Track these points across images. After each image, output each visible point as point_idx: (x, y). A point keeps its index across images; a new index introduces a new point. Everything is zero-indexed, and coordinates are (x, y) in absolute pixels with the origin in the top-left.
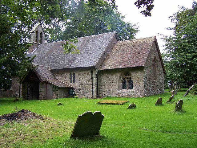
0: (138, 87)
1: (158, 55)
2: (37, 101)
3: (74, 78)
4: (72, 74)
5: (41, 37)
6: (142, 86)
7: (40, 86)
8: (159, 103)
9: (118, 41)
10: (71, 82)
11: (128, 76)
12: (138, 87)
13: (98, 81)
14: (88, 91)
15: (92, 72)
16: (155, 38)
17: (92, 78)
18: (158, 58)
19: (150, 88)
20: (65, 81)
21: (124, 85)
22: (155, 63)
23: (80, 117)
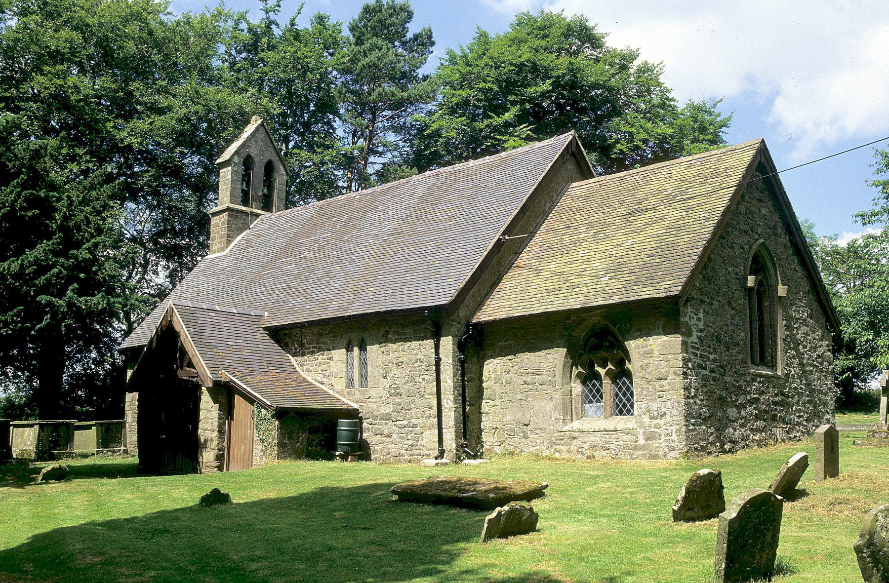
0: (654, 406)
1: (784, 239)
10: (350, 383)
21: (624, 395)
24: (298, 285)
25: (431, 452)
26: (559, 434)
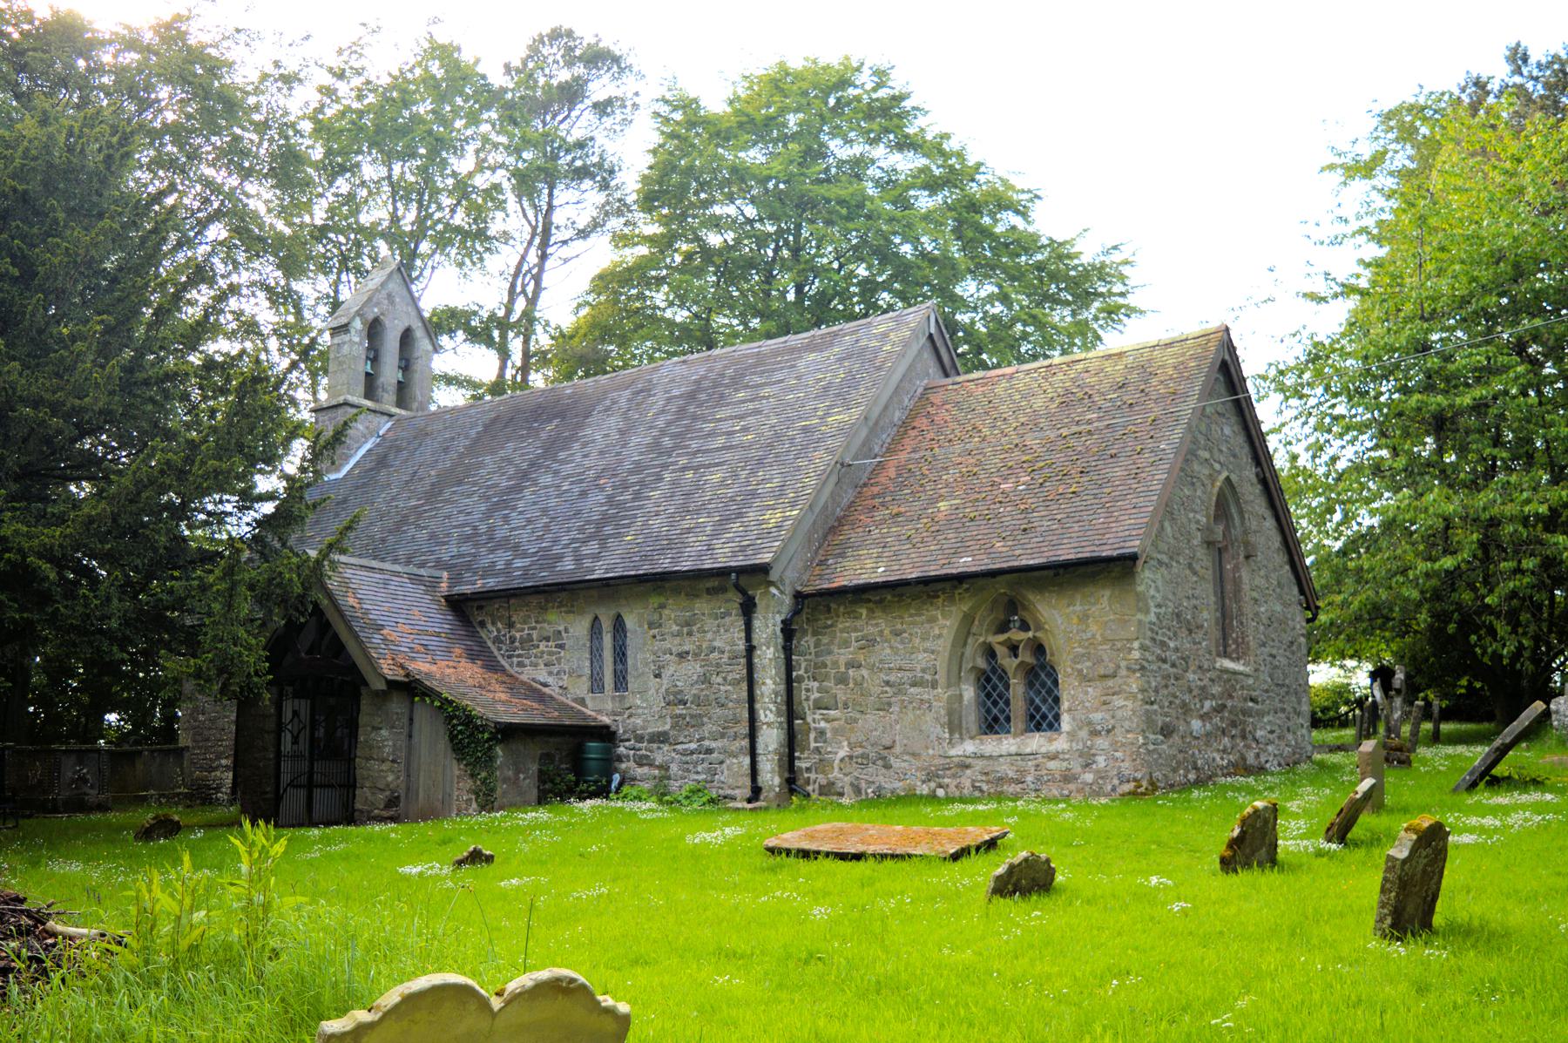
0: (1097, 717)
1: (1250, 472)
3: (620, 655)
8: (1253, 846)
9: (947, 375)
10: (596, 685)
11: (1016, 635)
14: (724, 751)
16: (1227, 329)
17: (750, 650)
18: (1251, 492)
19: (1196, 724)
20: (557, 672)
21: (995, 703)
22: (1227, 528)
24: (491, 529)
25: (737, 792)
26: (943, 761)
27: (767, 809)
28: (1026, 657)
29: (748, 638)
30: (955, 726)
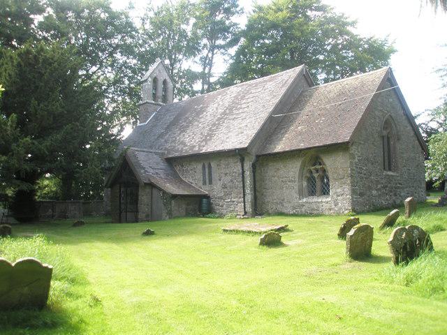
2: (119, 225)
4: (206, 166)
5: (165, 89)
6: (347, 189)
7: (141, 192)
10: (204, 183)
11: (318, 167)
12: (339, 190)
13: (257, 178)
15: (242, 161)
17: (243, 172)
19: (374, 192)
20: (194, 181)
23: (391, 242)
27: (248, 218)
28: (321, 173)
29: (243, 170)
30: (301, 194)
